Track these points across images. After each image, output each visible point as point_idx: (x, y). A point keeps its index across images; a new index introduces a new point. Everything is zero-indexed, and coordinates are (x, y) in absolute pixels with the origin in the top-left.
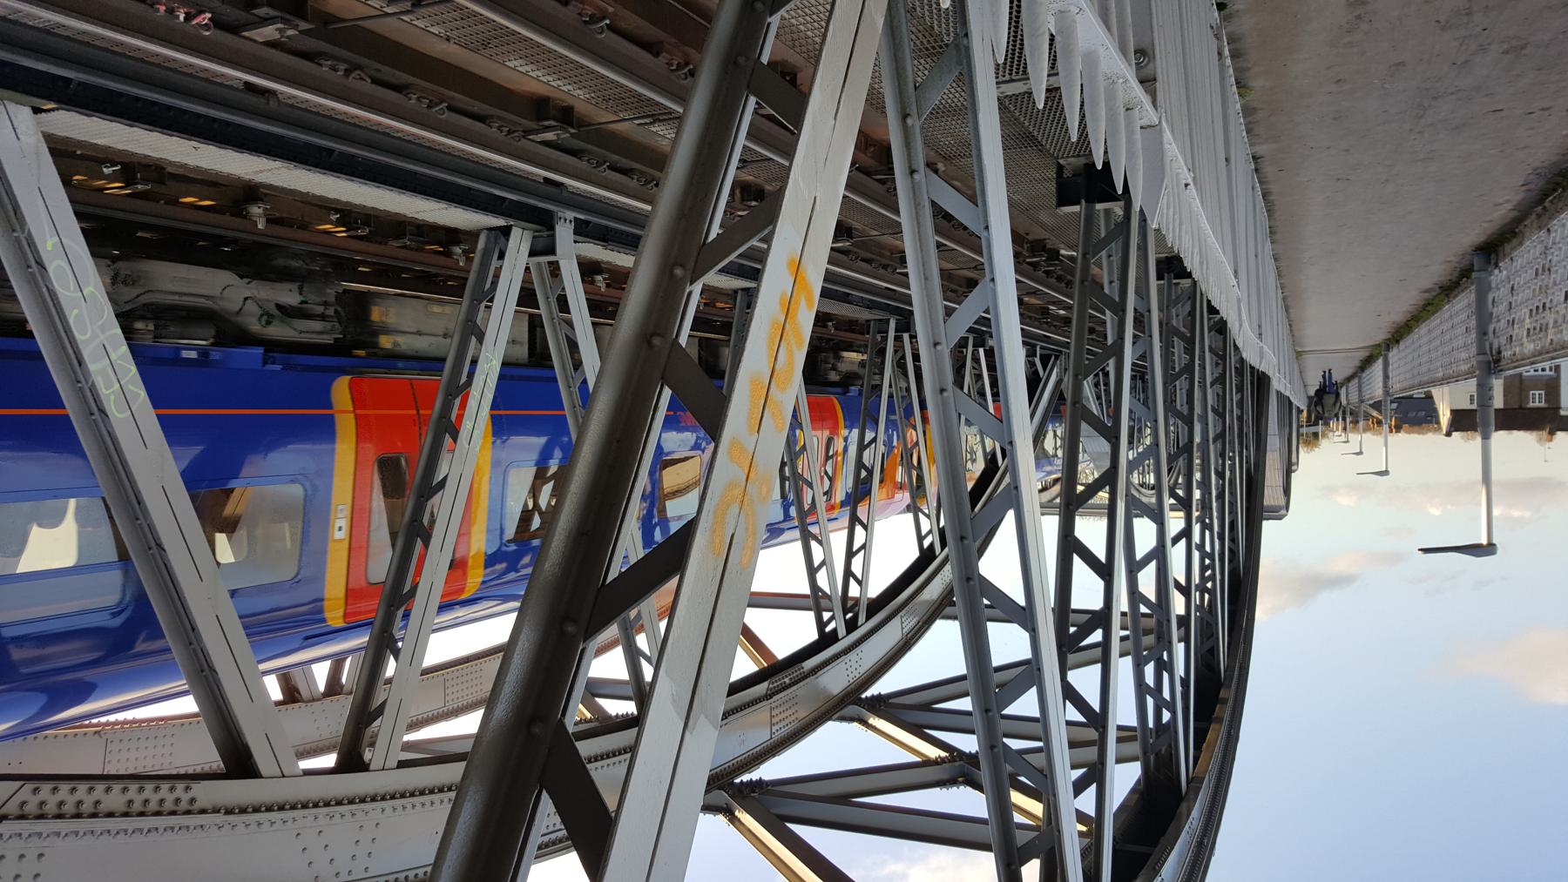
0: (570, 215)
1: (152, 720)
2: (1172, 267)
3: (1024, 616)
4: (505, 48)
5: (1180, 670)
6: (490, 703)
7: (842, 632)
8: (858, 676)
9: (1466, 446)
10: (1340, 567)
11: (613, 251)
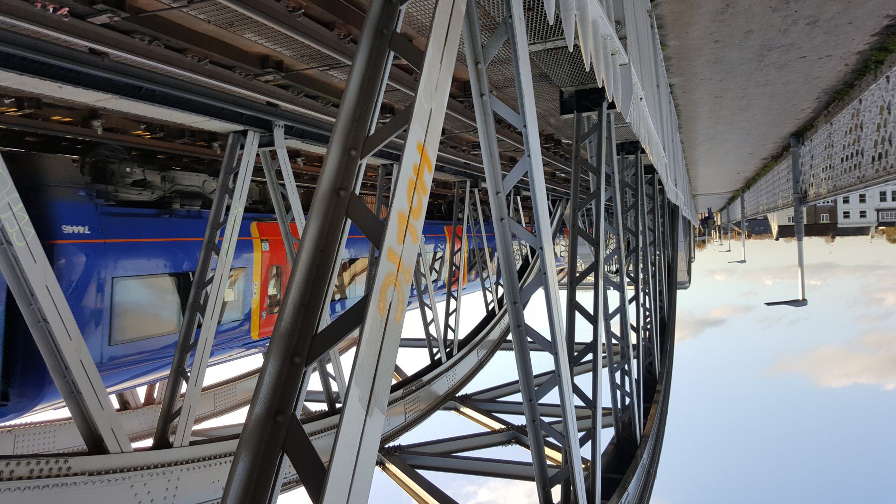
0: (282, 123)
2: (631, 147)
3: (550, 347)
4: (243, 27)
5: (635, 375)
6: (253, 402)
7: (444, 359)
8: (454, 384)
9: (789, 246)
10: (716, 314)
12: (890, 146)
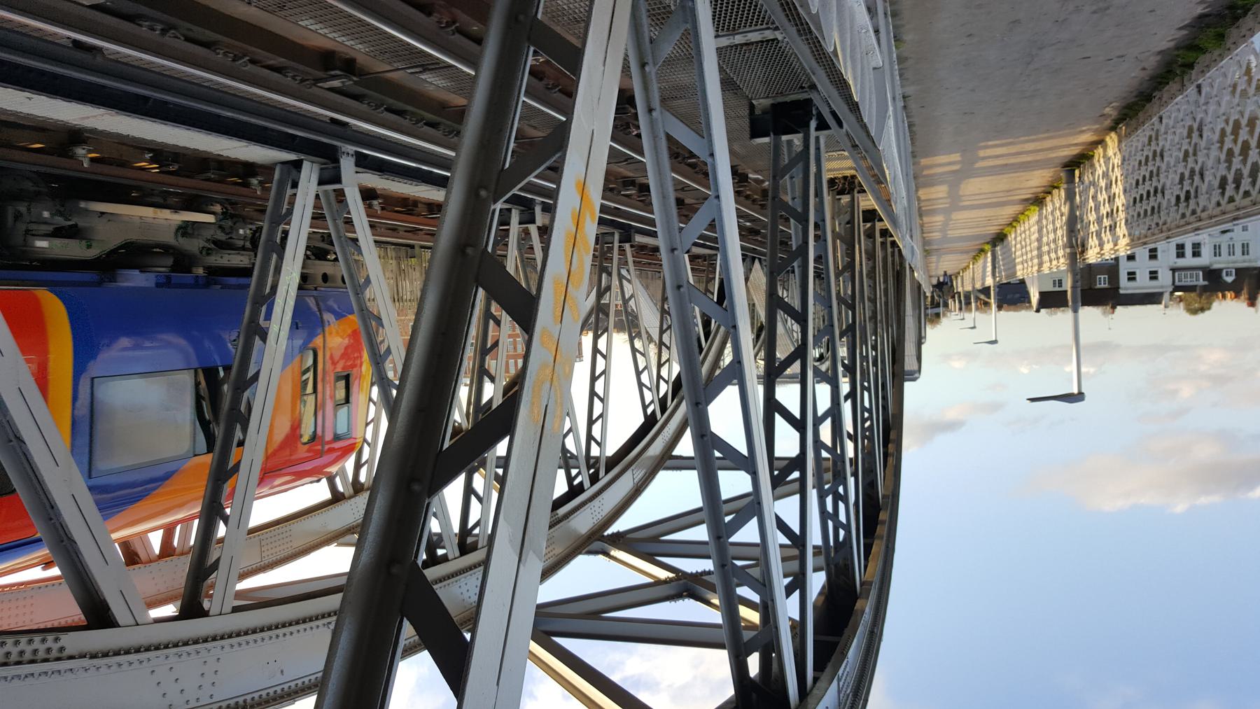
0: (351, 149)
1: (21, 584)
3: (746, 463)
4: (297, 10)
7: (587, 484)
8: (601, 518)
9: (1063, 317)
10: (951, 415)
11: (388, 179)
12: (1201, 182)
